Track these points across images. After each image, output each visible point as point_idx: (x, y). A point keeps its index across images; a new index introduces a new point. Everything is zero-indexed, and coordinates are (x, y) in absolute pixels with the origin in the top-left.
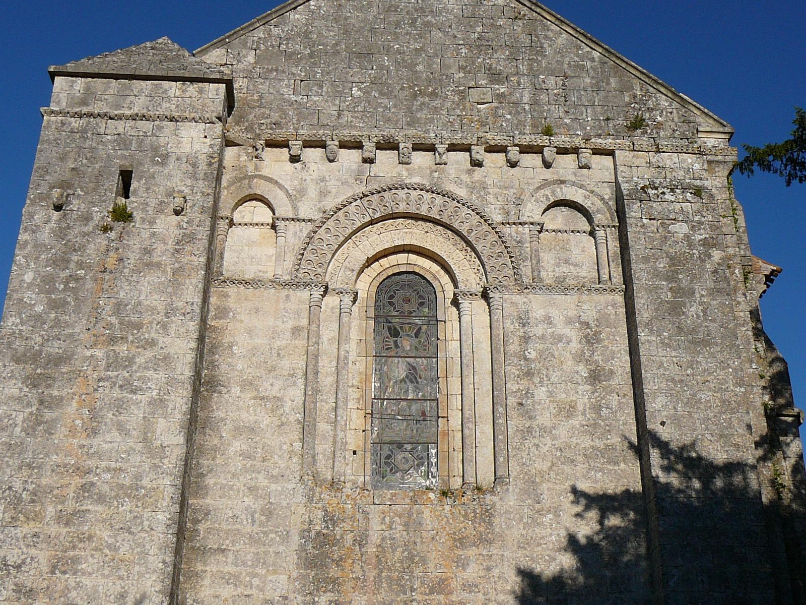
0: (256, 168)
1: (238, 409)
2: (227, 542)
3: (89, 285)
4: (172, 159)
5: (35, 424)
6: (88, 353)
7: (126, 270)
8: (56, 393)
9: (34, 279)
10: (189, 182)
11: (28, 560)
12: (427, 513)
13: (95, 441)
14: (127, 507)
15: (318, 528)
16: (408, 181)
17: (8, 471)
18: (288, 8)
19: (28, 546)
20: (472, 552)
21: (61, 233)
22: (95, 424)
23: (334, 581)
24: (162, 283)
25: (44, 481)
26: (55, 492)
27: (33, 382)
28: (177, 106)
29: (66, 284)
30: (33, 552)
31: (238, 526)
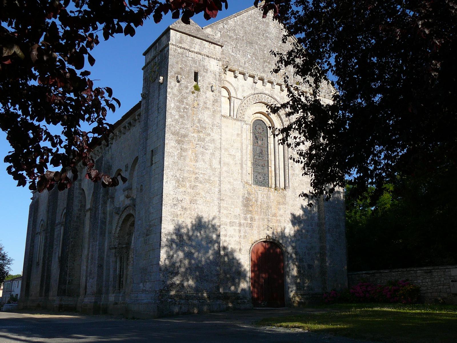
0: (225, 78)
1: (224, 157)
2: (224, 197)
3: (190, 111)
4: (209, 71)
5: (180, 156)
6: (192, 135)
7: (200, 108)
8: (185, 147)
9: (174, 106)
10: (214, 81)
11: (184, 199)
12: (271, 195)
13: (197, 164)
14: (208, 186)
15: (246, 196)
16: (265, 92)
17: (175, 170)
18: (229, 19)
19: (183, 195)
20: (281, 206)
21: (180, 91)
22: (197, 159)
23: (251, 211)
24: (210, 115)
25: (185, 175)
26: (188, 179)
27: (178, 142)
28: (208, 52)
29: (184, 110)
30: (185, 197)
31: (226, 193)
